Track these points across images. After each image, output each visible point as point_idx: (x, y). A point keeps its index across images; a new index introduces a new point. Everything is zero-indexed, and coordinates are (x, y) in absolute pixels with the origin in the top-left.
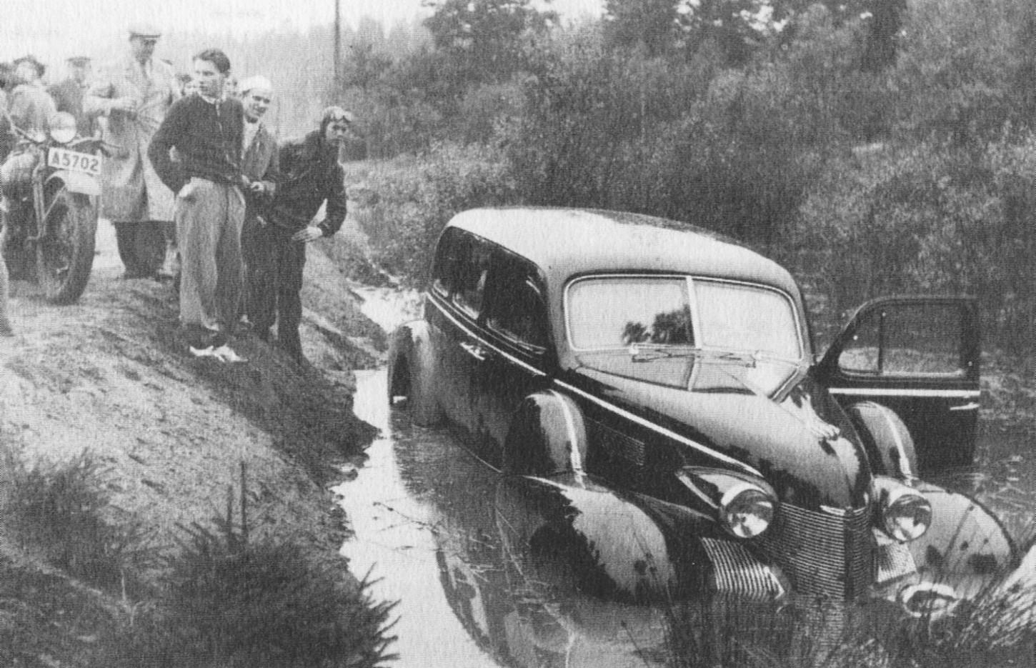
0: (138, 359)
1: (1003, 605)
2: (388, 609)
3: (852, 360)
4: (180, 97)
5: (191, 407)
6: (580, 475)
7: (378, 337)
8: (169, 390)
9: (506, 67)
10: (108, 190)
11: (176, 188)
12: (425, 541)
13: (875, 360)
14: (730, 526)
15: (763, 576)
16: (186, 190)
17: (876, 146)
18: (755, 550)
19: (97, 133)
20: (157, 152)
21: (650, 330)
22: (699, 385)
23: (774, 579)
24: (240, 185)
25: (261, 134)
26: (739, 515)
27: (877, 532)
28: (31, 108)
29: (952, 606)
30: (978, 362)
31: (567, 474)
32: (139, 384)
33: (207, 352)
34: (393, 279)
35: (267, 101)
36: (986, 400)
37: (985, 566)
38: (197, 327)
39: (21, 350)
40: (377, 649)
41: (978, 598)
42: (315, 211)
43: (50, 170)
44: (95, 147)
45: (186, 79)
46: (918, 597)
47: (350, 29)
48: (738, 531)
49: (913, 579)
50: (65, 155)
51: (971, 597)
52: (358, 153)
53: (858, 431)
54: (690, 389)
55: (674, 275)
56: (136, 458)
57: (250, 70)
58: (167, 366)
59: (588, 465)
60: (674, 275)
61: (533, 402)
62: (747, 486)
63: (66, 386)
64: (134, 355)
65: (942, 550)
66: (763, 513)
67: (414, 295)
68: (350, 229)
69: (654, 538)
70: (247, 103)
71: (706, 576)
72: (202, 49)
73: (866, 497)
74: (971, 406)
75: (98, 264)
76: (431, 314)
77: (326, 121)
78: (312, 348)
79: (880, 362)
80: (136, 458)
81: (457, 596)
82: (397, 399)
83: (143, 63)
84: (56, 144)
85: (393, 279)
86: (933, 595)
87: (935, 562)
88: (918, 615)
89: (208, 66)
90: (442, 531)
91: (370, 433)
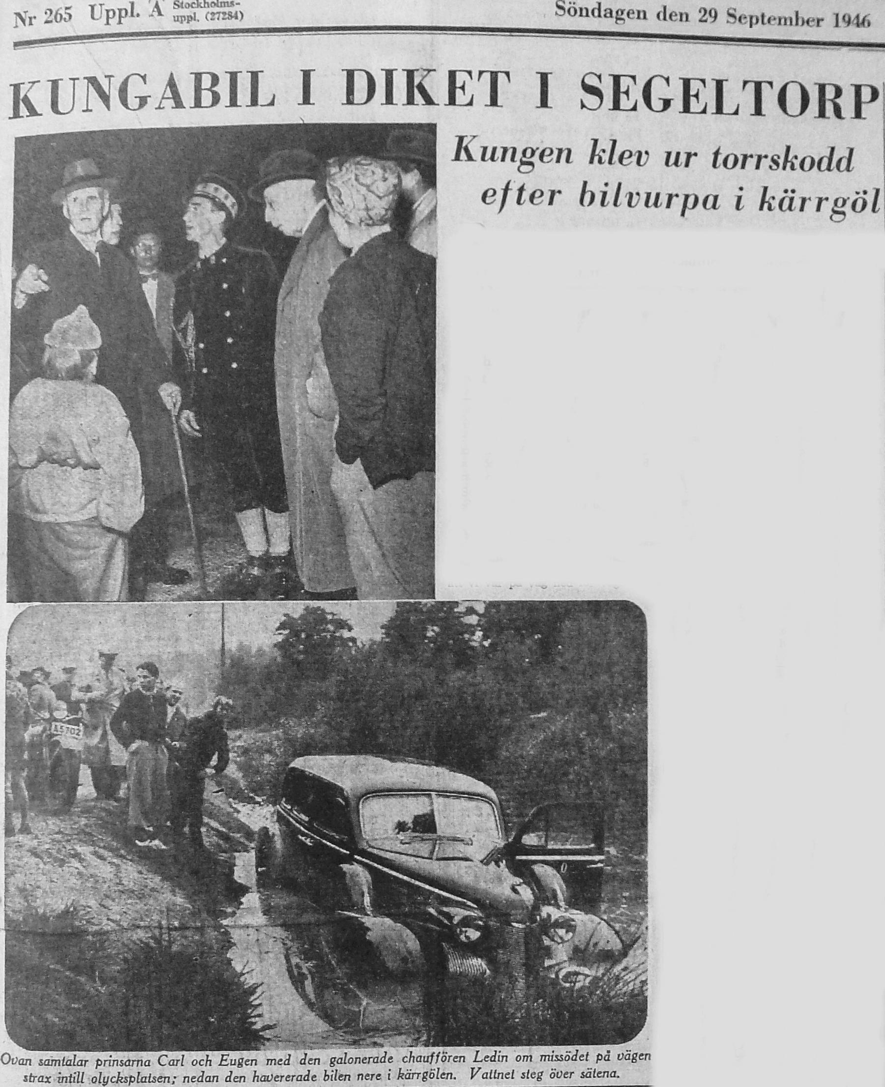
0: (104, 848)
1: (618, 979)
2: (256, 988)
3: (531, 839)
4: (128, 691)
5: (136, 875)
6: (369, 910)
7: (249, 834)
8: (124, 866)
9: (323, 668)
10: (88, 748)
11: (126, 745)
12: (279, 948)
13: (543, 839)
14: (458, 936)
15: (477, 964)
16: (134, 746)
17: (543, 714)
18: (472, 949)
19: (80, 713)
20: (115, 724)
21: (410, 825)
22: (440, 856)
23: (484, 966)
24: (165, 742)
25: (178, 712)
26: (464, 929)
27: (544, 937)
28: (41, 698)
29: (588, 980)
30: (602, 841)
31: (362, 911)
32: (106, 863)
33: (146, 843)
34: (258, 799)
35: (180, 693)
36: (608, 862)
37: (609, 957)
38: (139, 829)
39: (35, 842)
40: (249, 1011)
41: (604, 975)
42: (210, 760)
43: (51, 736)
44: (76, 722)
45: (131, 680)
46: (569, 974)
47: (230, 650)
48: (463, 938)
49: (566, 964)
50: (61, 727)
51: (599, 974)
52: (235, 724)
53: (532, 880)
54: (434, 857)
55: (425, 792)
56: (103, 906)
57: (172, 674)
58: (122, 852)
59: (373, 904)
60: (425, 792)
61: (341, 869)
62: (467, 913)
63: (62, 863)
64: (102, 845)
65: (582, 947)
66: (478, 928)
67: (271, 808)
68: (232, 770)
69: (413, 943)
70: (169, 694)
71: (222, 181)
72: (142, 662)
73: (538, 917)
74: (600, 865)
75: (81, 792)
76: (281, 819)
77: (218, 703)
78: (208, 840)
79: (546, 841)
80: (103, 906)
81: (297, 980)
82: (259, 870)
83: (107, 672)
84: (56, 720)
85: (258, 799)
86: (577, 974)
87: (579, 955)
88: (568, 985)
89: (146, 673)
90: (289, 943)
91: (244, 890)
